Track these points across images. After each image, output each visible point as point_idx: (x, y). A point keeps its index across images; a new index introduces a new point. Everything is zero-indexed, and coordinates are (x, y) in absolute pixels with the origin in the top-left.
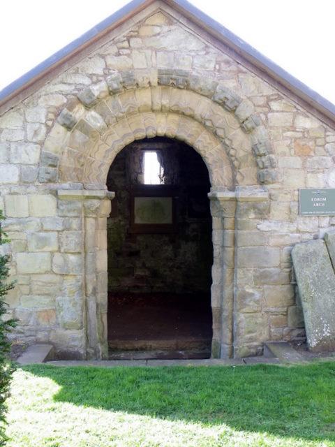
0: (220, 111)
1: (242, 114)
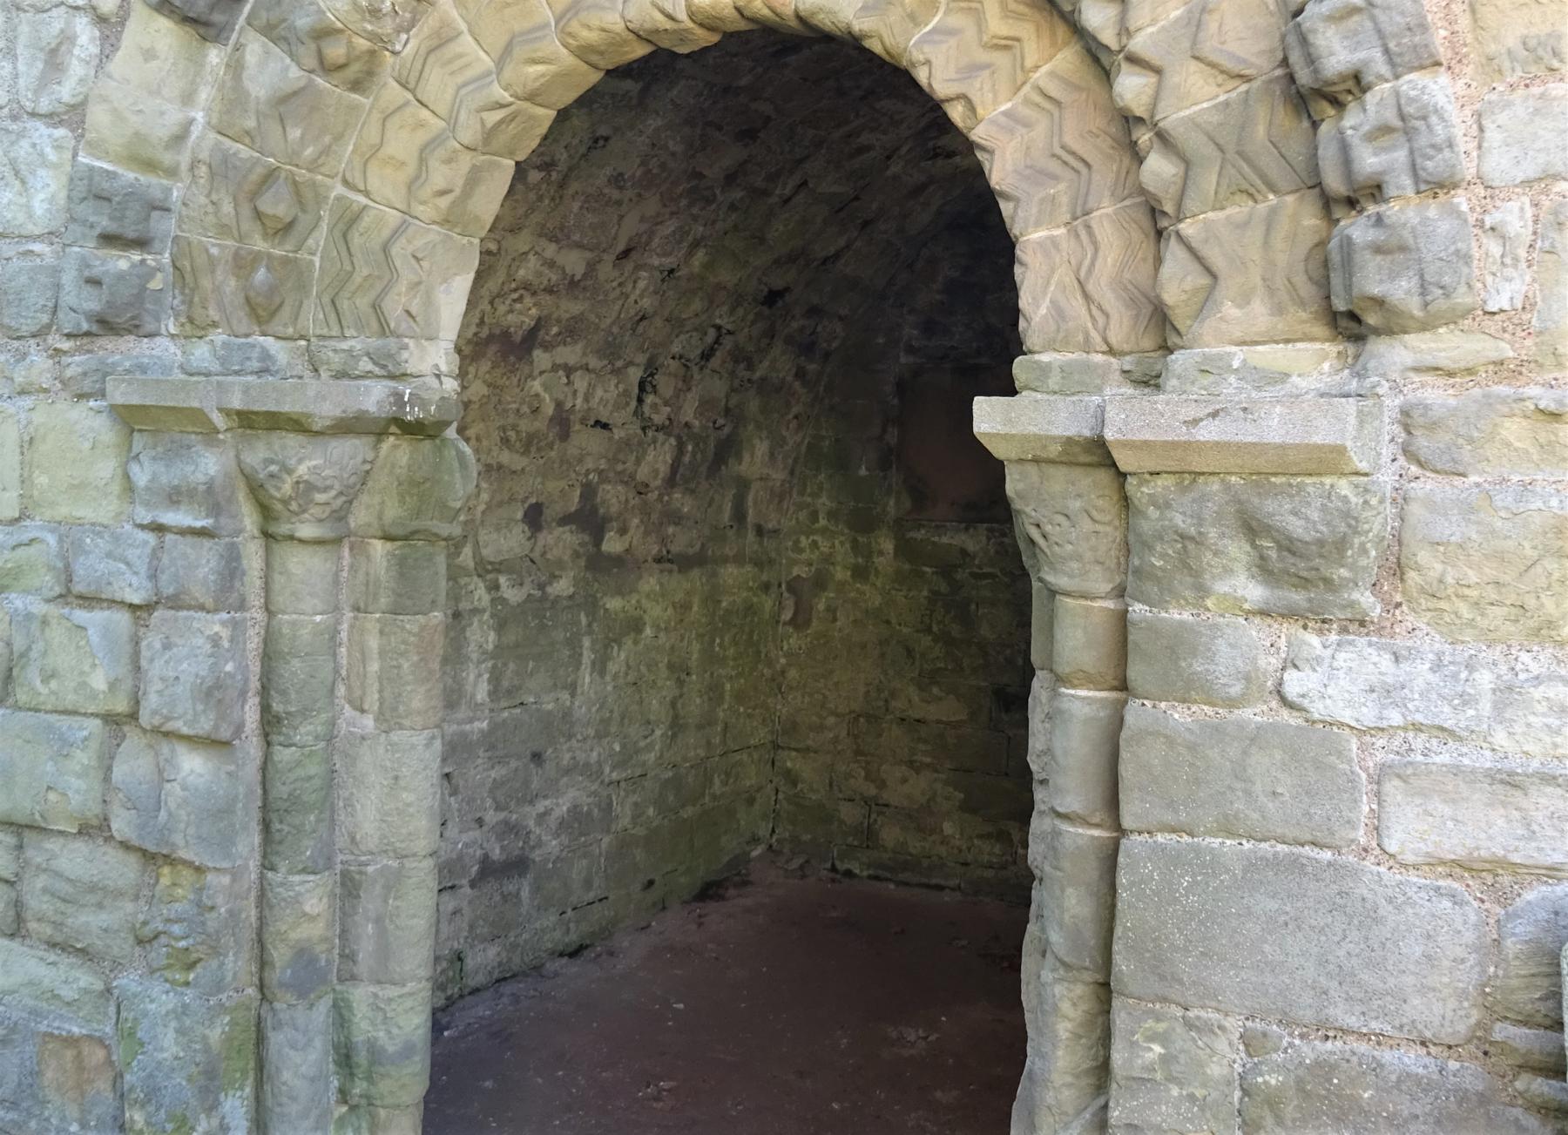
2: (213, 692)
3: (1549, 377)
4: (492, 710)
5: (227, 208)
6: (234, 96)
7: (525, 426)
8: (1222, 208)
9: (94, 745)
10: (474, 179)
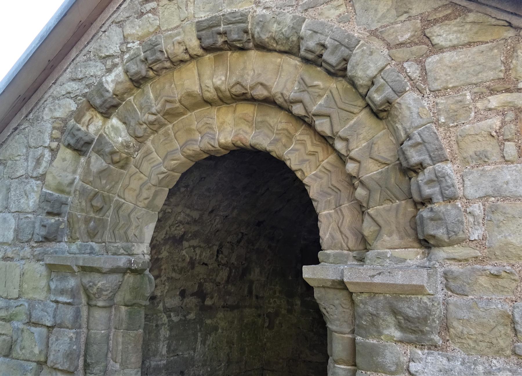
0: (320, 81)
1: (360, 74)
2: (69, 355)
3: (494, 262)
4: (167, 357)
5: (84, 204)
6: (87, 171)
7: (180, 265)
8: (382, 205)
9: (33, 372)
10: (156, 194)
